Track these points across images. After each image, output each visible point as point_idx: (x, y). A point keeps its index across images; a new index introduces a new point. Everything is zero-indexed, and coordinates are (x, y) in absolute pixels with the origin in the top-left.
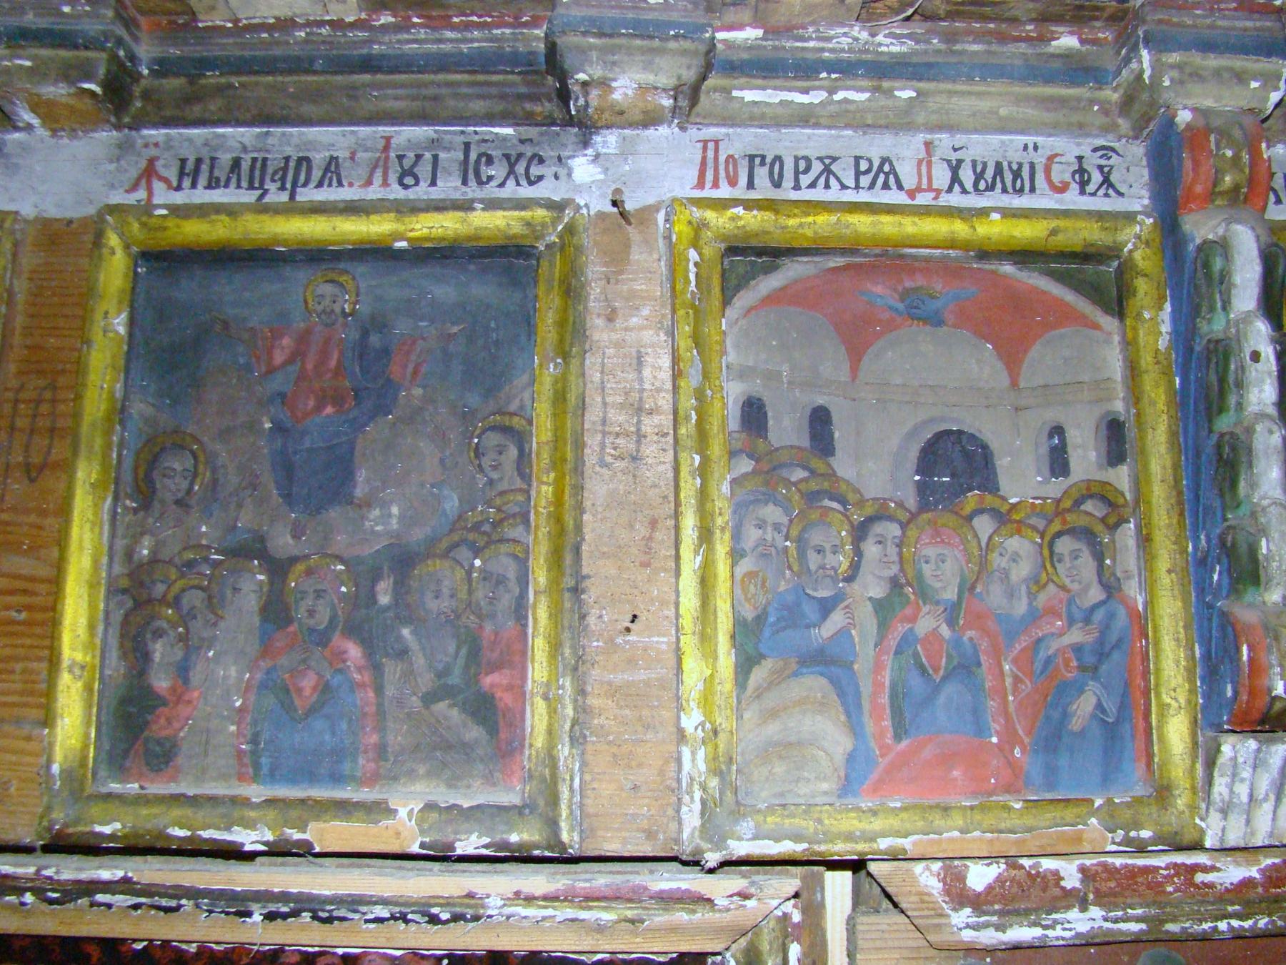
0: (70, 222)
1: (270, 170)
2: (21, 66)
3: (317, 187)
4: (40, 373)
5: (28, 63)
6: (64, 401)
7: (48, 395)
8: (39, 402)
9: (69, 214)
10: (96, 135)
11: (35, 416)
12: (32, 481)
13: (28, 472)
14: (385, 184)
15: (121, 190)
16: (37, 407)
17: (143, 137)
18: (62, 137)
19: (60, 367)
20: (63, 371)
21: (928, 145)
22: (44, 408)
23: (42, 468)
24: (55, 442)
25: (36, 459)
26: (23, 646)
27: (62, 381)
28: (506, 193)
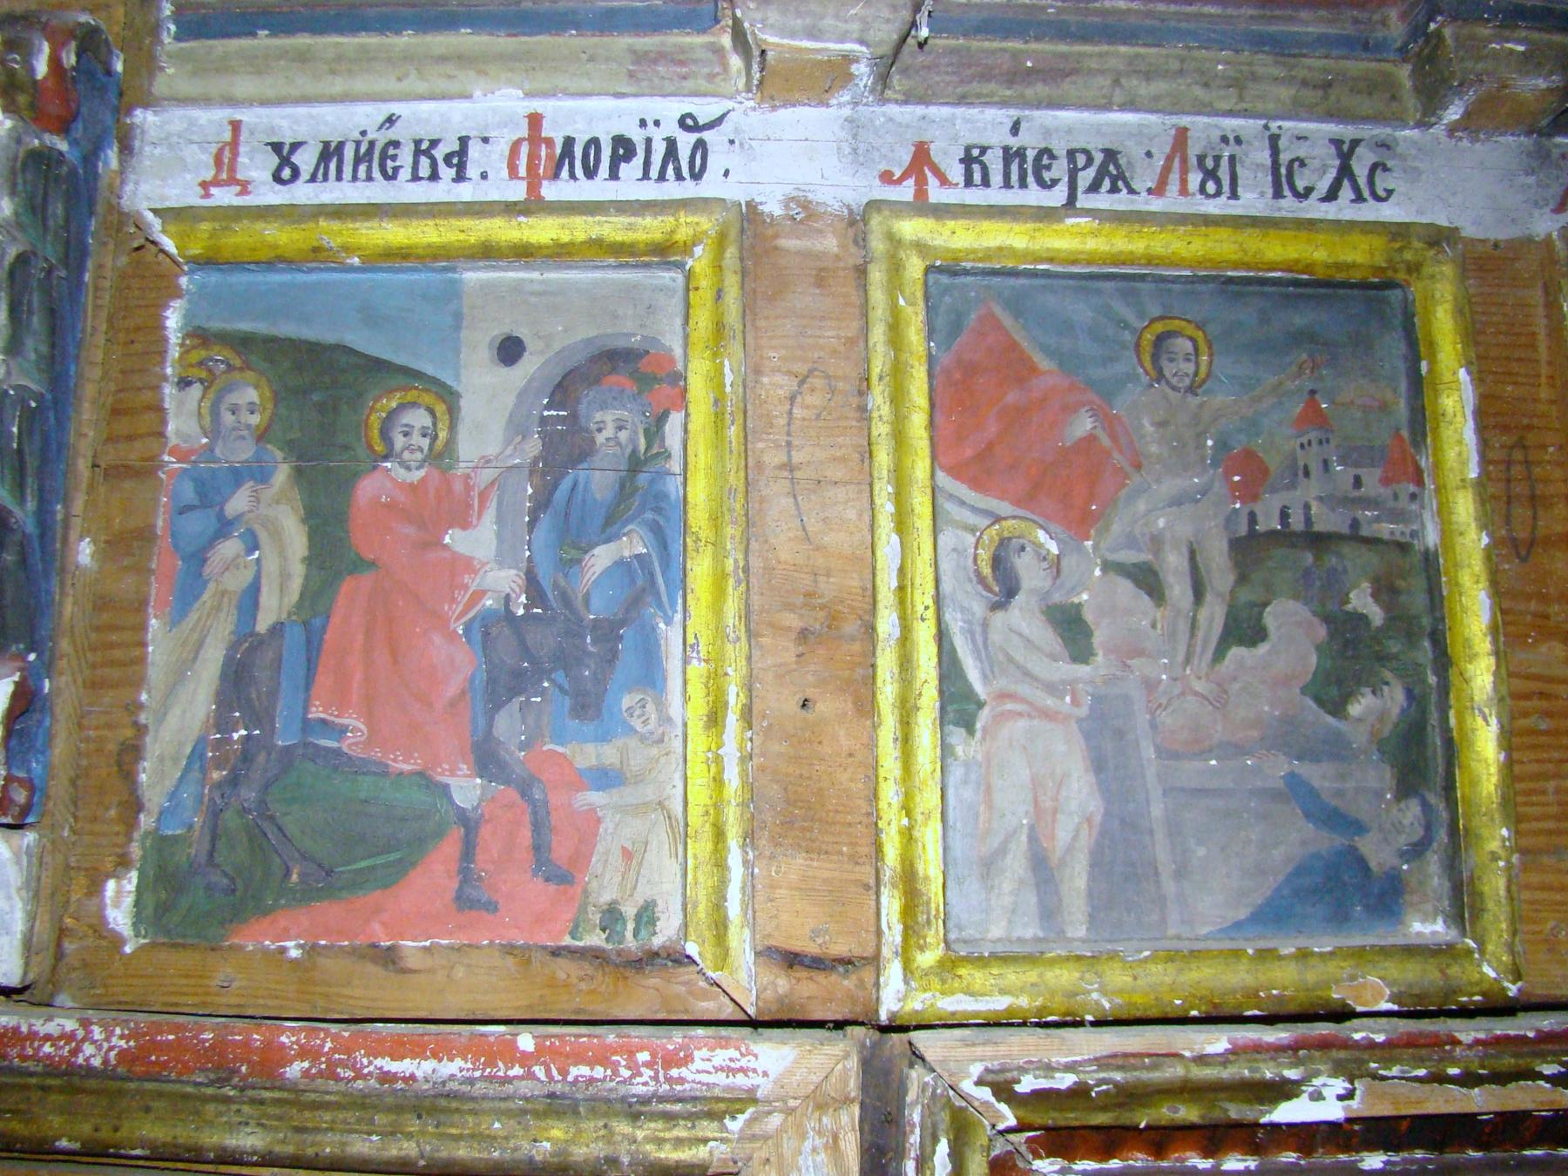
0: (1496, 245)
1: (639, 160)
2: (1511, 52)
3: (1323, 200)
4: (1506, 429)
5: (1521, 48)
6: (1539, 463)
7: (1518, 455)
8: (1509, 463)
9: (1492, 235)
10: (1501, 139)
11: (1508, 481)
12: (1524, 560)
13: (1516, 547)
14: (1184, 191)
15: (1547, 210)
16: (1508, 469)
17: (1558, 146)
18: (1461, 139)
19: (1525, 421)
20: (1529, 428)
21: (236, 126)
22: (1517, 470)
23: (1532, 544)
24: (1541, 513)
25: (1522, 534)
26: (1550, 761)
27: (1531, 438)
28: (1329, 211)
